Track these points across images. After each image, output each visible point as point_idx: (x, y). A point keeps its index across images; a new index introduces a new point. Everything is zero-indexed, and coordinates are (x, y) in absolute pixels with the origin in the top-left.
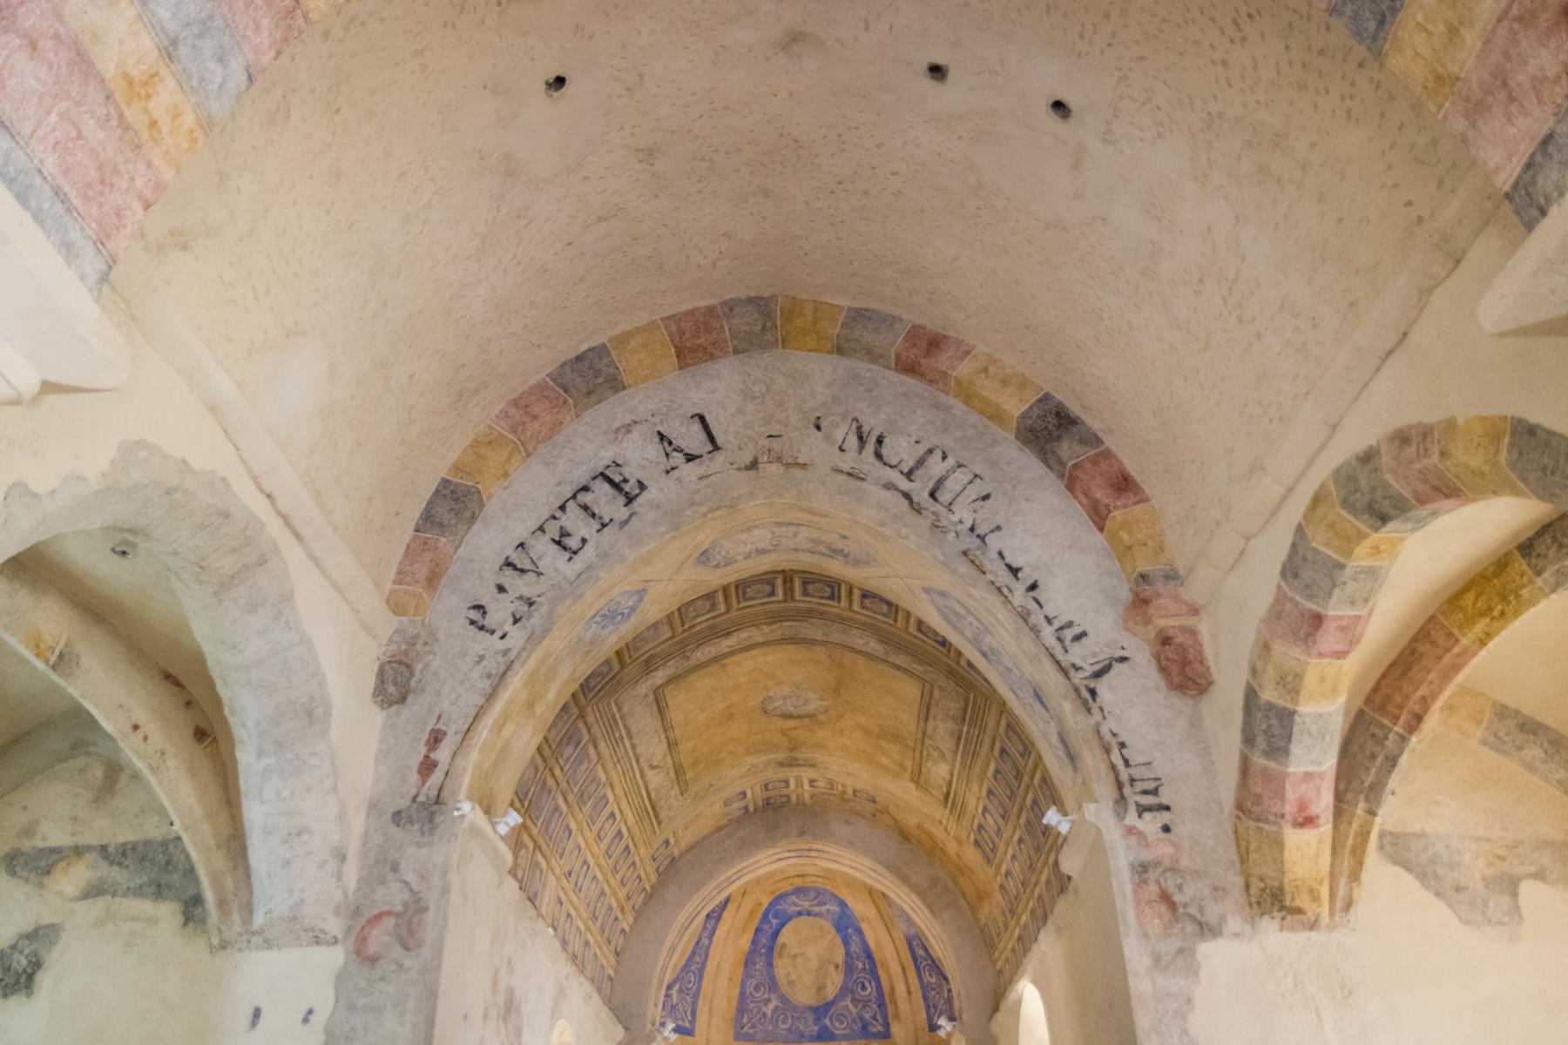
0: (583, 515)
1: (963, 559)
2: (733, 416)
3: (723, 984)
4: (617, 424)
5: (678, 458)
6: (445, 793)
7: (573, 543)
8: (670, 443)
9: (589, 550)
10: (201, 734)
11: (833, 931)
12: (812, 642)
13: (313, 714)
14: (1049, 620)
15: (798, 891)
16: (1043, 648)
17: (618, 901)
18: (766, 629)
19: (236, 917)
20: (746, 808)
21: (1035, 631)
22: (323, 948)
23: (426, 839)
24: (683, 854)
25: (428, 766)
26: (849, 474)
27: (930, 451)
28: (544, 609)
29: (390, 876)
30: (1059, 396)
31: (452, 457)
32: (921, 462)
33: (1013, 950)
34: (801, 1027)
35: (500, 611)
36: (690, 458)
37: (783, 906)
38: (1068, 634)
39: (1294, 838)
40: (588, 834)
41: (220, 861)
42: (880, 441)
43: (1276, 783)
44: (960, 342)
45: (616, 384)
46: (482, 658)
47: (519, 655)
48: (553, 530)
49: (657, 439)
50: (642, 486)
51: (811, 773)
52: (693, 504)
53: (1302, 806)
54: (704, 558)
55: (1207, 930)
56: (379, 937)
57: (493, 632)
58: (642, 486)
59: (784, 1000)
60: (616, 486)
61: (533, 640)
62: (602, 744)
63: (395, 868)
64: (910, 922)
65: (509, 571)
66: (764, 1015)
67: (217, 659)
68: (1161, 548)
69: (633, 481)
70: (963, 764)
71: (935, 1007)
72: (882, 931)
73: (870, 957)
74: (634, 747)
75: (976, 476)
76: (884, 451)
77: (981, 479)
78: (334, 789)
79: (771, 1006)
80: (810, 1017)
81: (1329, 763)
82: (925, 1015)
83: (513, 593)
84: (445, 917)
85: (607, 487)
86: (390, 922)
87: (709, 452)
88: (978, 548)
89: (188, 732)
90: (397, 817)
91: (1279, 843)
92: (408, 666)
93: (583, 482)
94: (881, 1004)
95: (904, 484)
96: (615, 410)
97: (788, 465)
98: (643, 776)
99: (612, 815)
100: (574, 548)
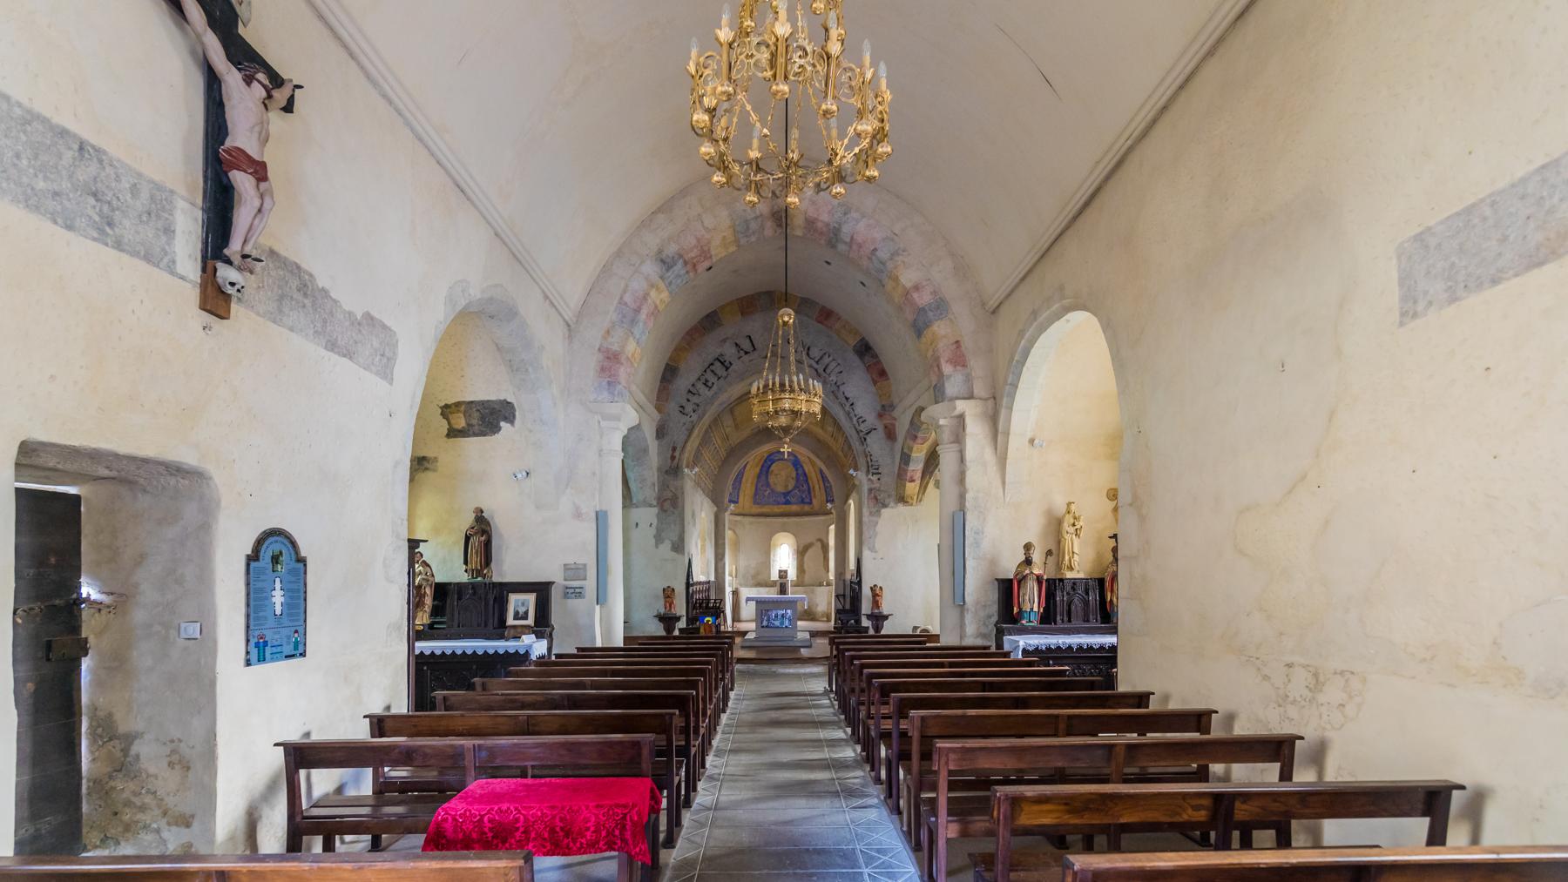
0: (712, 374)
3: (749, 485)
4: (721, 339)
5: (742, 353)
7: (710, 384)
11: (792, 467)
14: (855, 416)
21: (851, 419)
25: (673, 458)
27: (825, 354)
30: (867, 338)
32: (821, 358)
34: (779, 499)
35: (689, 408)
36: (746, 353)
37: (772, 457)
38: (861, 420)
39: (908, 485)
42: (809, 349)
43: (906, 471)
44: (837, 315)
46: (685, 424)
50: (731, 364)
53: (911, 477)
55: (885, 506)
58: (731, 364)
59: (772, 491)
61: (700, 418)
63: (668, 487)
68: (890, 396)
72: (811, 468)
73: (805, 474)
76: (810, 353)
81: (920, 466)
85: (720, 364)
86: (669, 501)
90: (667, 472)
91: (905, 486)
94: (809, 493)
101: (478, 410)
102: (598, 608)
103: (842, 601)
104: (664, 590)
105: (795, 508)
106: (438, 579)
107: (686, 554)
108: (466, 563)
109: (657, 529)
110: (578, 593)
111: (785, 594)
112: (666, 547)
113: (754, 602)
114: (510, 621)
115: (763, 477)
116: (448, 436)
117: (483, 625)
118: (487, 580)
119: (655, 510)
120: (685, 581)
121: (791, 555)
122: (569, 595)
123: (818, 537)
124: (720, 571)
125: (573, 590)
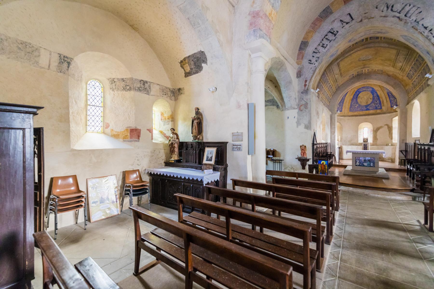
1: (412, 28)
2: (356, 11)
4: (332, 21)
6: (308, 89)
7: (325, 46)
8: (343, 21)
9: (328, 46)
10: (276, 87)
11: (370, 93)
12: (371, 47)
13: (290, 82)
15: (363, 88)
16: (431, 43)
17: (330, 95)
18: (361, 47)
19: (284, 107)
20: (353, 76)
22: (295, 110)
23: (307, 95)
24: (341, 86)
25: (305, 85)
26: (384, 17)
27: (406, 5)
28: (321, 58)
29: (302, 100)
31: (303, 36)
32: (403, 9)
33: (414, 94)
35: (313, 60)
36: (347, 23)
37: (360, 90)
40: (325, 87)
41: (281, 101)
45: (331, 13)
46: (311, 68)
47: (317, 67)
48: (321, 44)
49: (340, 21)
50: (337, 32)
51: (368, 69)
52: (348, 33)
54: (350, 41)
56: (302, 108)
57: (313, 64)
58: (337, 32)
59: (359, 105)
60: (332, 33)
61: (320, 64)
62: (328, 74)
63: (303, 99)
64: (387, 89)
65: (314, 53)
66: (355, 107)
67: (277, 78)
69: (336, 31)
70: (406, 63)
71: (393, 103)
74: (333, 73)
75: (418, 8)
77: (420, 8)
78: (294, 91)
79: (357, 106)
80: (365, 107)
82: (390, 105)
83: (315, 57)
84: (311, 105)
85: (331, 34)
86: (303, 106)
87: (351, 21)
88: (417, 25)
89: (274, 87)
90: (302, 93)
92: (300, 72)
93: (326, 34)
94: (380, 103)
95: (398, 15)
96: (331, 18)
97: (369, 19)
98: (334, 76)
99: (329, 83)
100: (325, 47)
101: (192, 60)
102: (249, 157)
103: (404, 153)
104: (301, 146)
105: (371, 112)
106: (181, 140)
107: (312, 130)
108: (192, 133)
109: (297, 119)
110: (238, 148)
111: (366, 149)
112: (302, 127)
113: (351, 153)
114: (205, 162)
115: (355, 100)
116: (186, 76)
117: (194, 162)
118: (200, 141)
119: (297, 110)
120: (312, 142)
121: (369, 132)
122: (235, 149)
123: (385, 124)
124: (333, 139)
125: (236, 147)
